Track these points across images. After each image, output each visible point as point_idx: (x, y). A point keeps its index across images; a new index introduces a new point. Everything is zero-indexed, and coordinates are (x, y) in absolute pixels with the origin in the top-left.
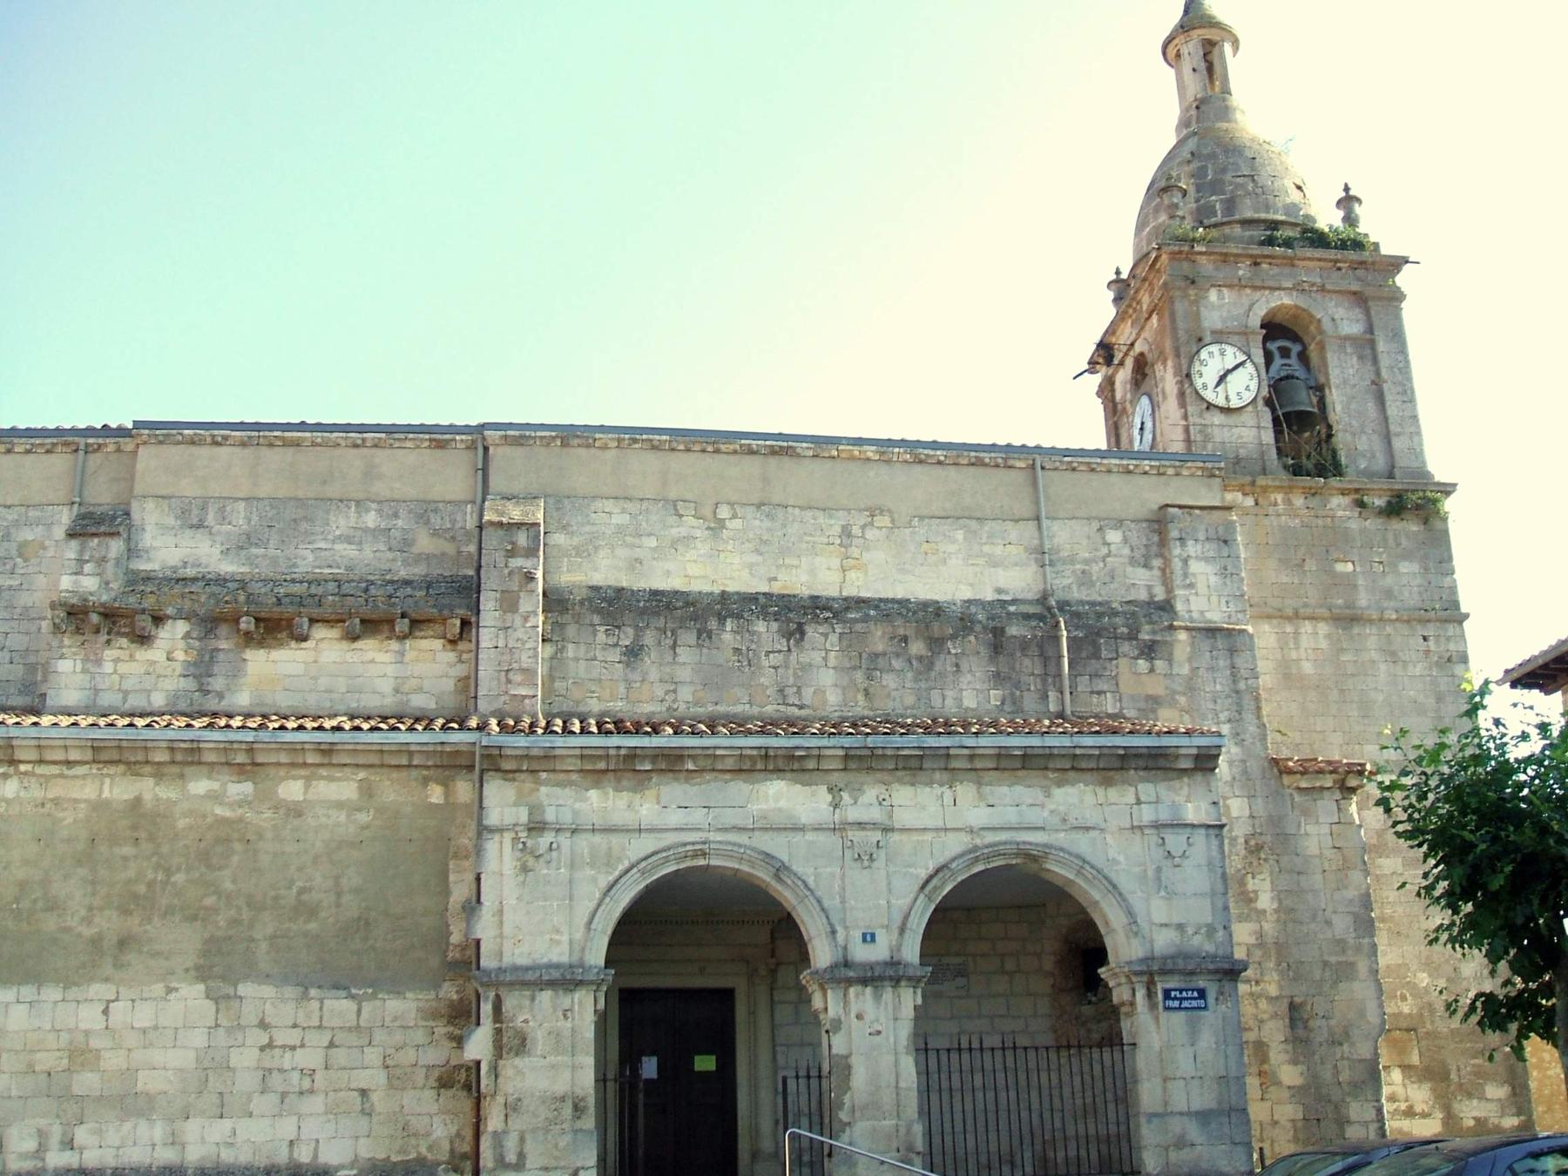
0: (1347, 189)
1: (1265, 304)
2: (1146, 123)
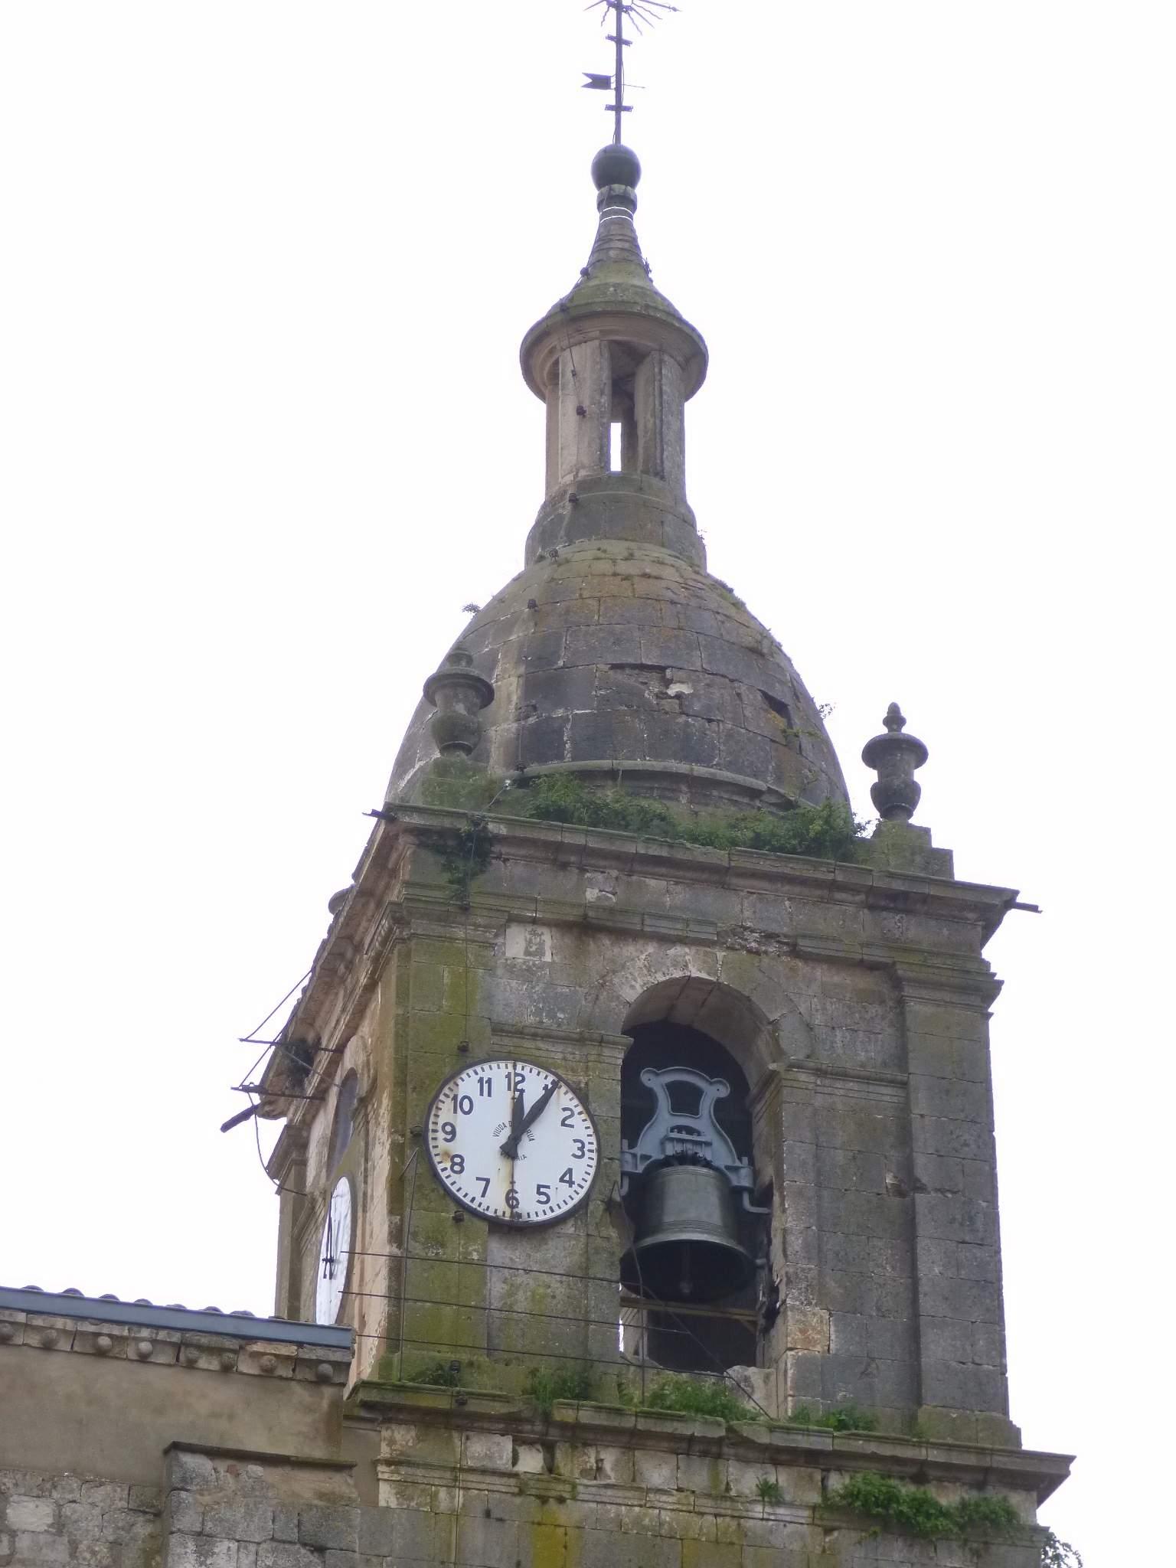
0: (894, 718)
1: (638, 972)
2: (466, 506)
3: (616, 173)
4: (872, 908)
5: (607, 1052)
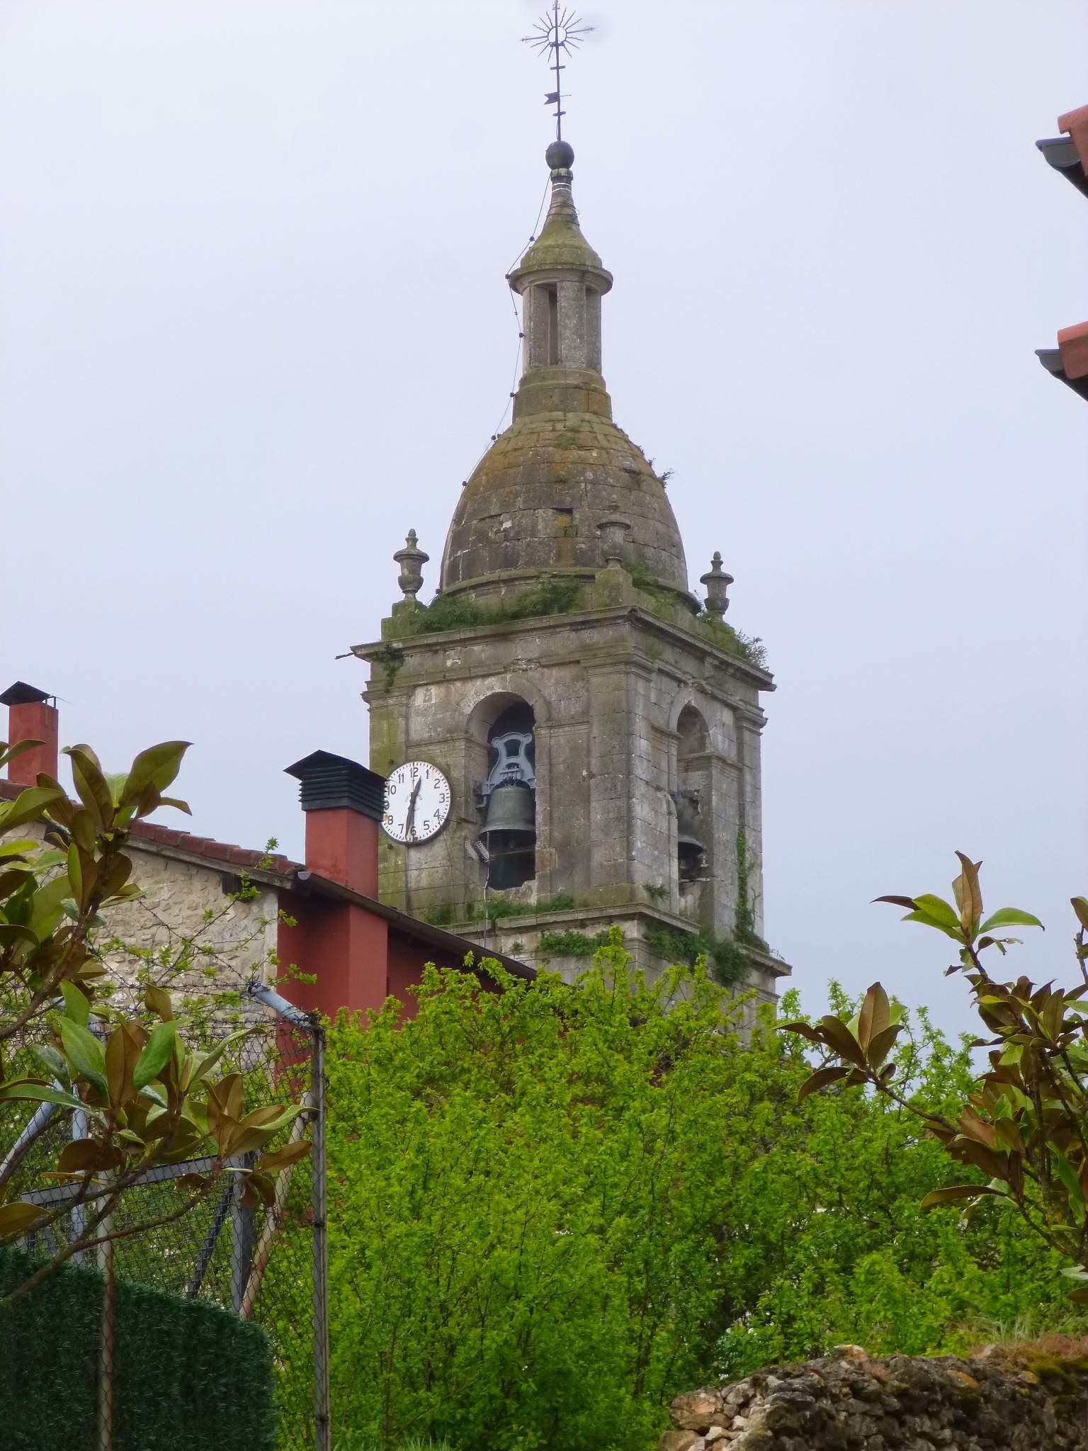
3: (561, 157)
4: (576, 630)
5: (457, 744)
